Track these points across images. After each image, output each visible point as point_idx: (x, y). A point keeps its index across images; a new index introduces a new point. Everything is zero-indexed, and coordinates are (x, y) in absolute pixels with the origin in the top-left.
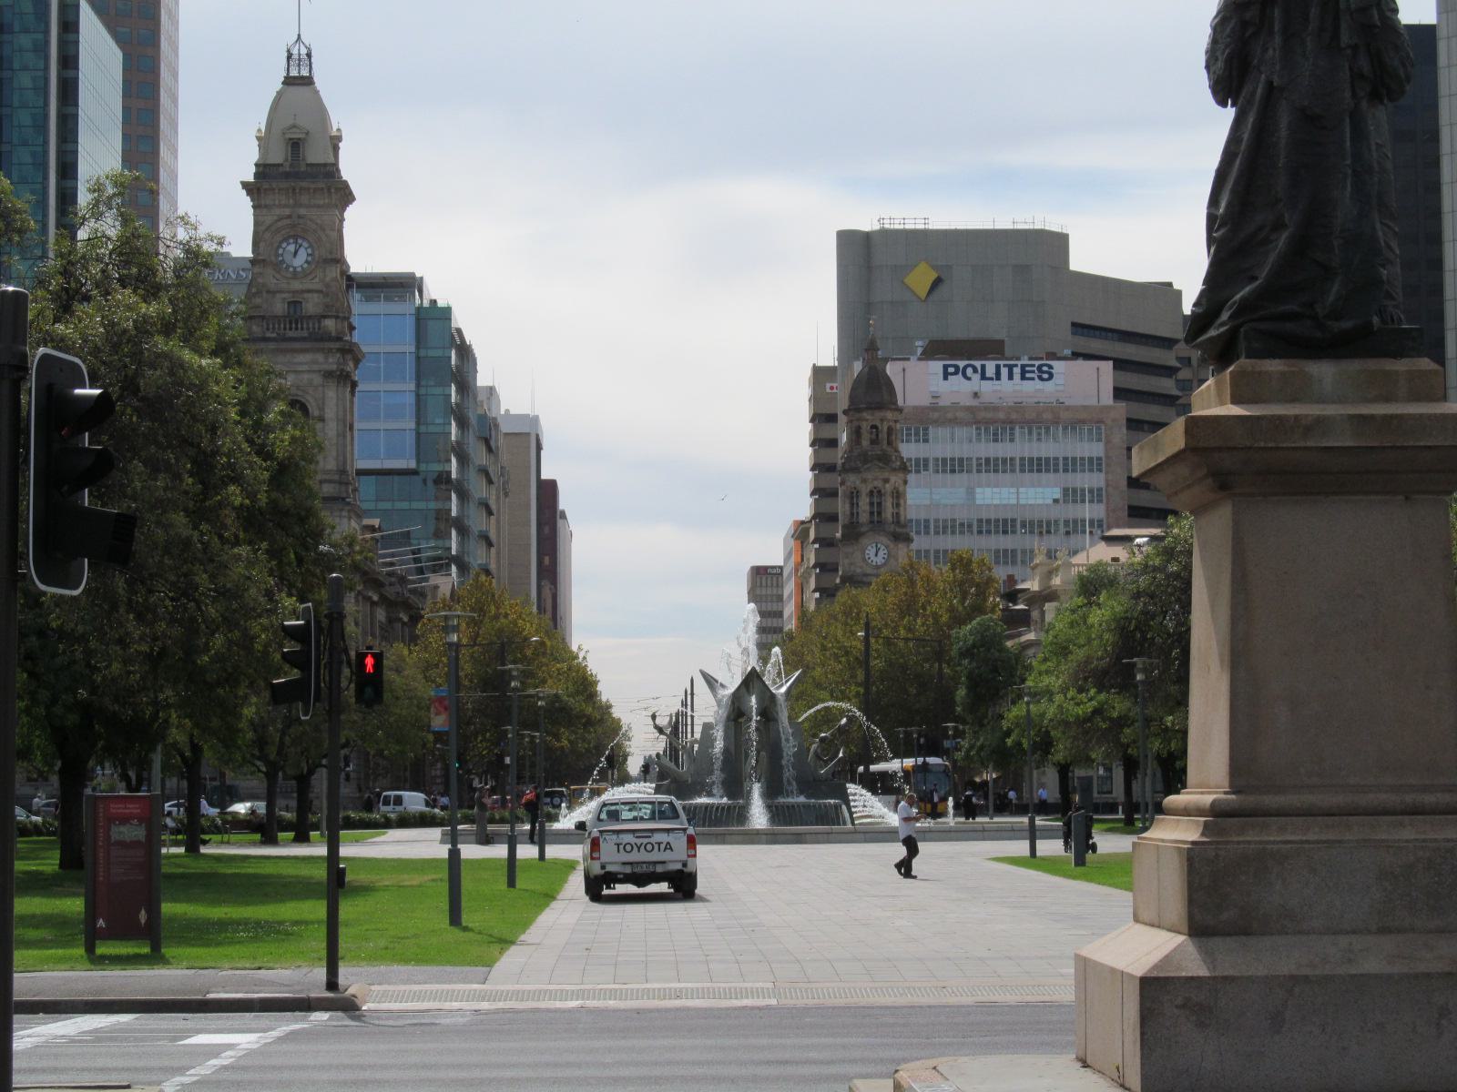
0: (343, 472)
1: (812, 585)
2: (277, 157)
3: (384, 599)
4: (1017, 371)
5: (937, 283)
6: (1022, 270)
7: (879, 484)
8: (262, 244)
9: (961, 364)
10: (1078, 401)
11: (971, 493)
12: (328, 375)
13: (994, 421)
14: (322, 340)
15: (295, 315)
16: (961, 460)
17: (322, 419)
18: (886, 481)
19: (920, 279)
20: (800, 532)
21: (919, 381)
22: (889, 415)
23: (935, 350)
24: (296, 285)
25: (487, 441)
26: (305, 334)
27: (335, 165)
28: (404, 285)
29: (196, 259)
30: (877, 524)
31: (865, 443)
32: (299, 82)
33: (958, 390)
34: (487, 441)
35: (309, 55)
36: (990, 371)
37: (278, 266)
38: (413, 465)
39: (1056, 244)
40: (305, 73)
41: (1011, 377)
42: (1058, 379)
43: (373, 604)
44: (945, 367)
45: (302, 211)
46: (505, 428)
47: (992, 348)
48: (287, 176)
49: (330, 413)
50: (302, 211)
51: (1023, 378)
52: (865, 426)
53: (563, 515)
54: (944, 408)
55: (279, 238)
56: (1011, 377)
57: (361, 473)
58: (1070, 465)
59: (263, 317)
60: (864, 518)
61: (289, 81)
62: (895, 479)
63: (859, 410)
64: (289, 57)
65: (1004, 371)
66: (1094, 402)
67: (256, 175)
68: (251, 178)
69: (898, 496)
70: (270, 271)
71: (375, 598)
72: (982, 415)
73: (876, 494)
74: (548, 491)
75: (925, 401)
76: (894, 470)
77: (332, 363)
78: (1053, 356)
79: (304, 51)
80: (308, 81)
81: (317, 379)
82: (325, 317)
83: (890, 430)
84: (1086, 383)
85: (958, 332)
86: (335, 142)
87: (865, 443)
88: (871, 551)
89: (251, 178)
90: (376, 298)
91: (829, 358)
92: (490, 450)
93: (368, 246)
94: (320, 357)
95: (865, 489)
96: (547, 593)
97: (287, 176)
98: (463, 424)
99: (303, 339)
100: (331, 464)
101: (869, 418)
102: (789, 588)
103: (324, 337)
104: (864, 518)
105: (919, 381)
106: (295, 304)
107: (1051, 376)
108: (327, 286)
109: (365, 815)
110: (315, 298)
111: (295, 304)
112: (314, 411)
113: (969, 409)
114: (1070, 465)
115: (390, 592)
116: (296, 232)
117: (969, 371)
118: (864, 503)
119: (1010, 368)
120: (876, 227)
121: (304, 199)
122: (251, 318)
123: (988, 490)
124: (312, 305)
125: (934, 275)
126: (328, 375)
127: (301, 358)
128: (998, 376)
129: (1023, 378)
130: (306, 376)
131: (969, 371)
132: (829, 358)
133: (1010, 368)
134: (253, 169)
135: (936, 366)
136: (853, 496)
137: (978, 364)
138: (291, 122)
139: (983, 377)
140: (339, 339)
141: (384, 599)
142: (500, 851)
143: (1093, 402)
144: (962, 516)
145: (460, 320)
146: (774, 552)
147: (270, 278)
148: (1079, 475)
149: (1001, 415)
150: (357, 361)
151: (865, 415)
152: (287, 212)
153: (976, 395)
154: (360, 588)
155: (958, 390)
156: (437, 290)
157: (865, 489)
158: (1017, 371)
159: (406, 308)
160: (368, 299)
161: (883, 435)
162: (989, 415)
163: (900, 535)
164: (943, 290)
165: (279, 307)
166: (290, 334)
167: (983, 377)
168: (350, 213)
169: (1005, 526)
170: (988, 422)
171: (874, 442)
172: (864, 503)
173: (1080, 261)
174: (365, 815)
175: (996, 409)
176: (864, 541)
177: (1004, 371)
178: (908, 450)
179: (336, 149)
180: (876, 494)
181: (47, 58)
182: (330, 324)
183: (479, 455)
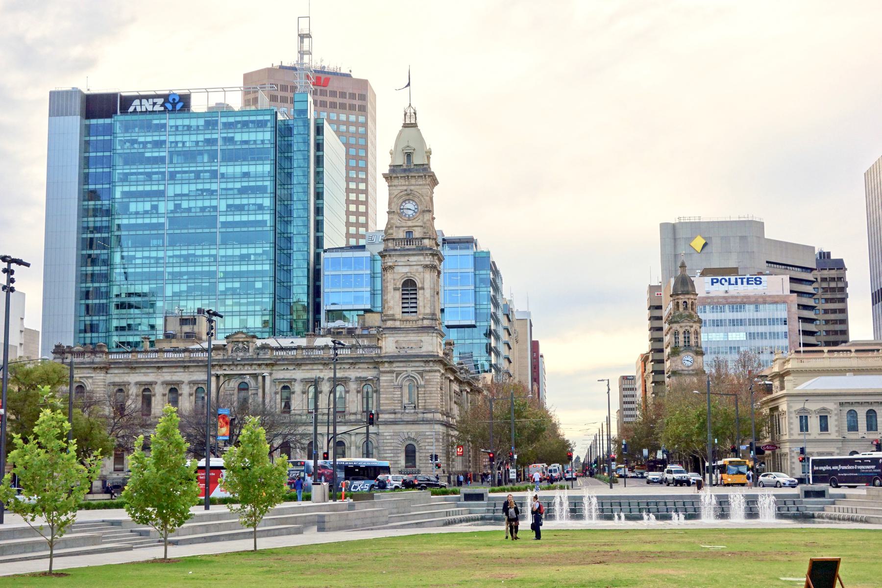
1: (651, 380)
2: (401, 160)
3: (456, 379)
4: (745, 280)
5: (705, 245)
7: (688, 328)
8: (393, 205)
9: (720, 278)
13: (736, 303)
14: (422, 250)
15: (409, 239)
16: (721, 320)
17: (423, 288)
18: (692, 327)
20: (645, 359)
22: (692, 297)
24: (410, 223)
25: (508, 316)
26: (414, 247)
27: (428, 165)
28: (468, 242)
30: (688, 347)
31: (681, 309)
32: (410, 125)
33: (718, 290)
34: (508, 316)
35: (415, 113)
36: (733, 281)
38: (473, 323)
40: (413, 122)
41: (742, 283)
43: (451, 381)
44: (712, 280)
45: (412, 188)
48: (405, 170)
50: (412, 188)
51: (748, 283)
52: (681, 302)
53: (542, 356)
54: (712, 297)
55: (401, 201)
56: (742, 283)
57: (448, 327)
59: (393, 239)
60: (681, 344)
61: (405, 126)
63: (678, 295)
64: (405, 114)
65: (739, 281)
66: (781, 293)
67: (390, 170)
68: (387, 172)
69: (697, 333)
71: (452, 378)
72: (730, 300)
76: (695, 322)
77: (428, 260)
78: (761, 273)
79: (412, 111)
80: (414, 125)
81: (420, 269)
82: (423, 238)
83: (692, 304)
84: (777, 284)
85: (715, 265)
86: (429, 153)
87: (681, 309)
89: (387, 172)
92: (509, 320)
94: (421, 258)
95: (681, 331)
96: (535, 387)
98: (496, 305)
99: (414, 249)
101: (682, 298)
102: (639, 383)
103: (423, 248)
104: (681, 344)
107: (761, 283)
108: (425, 223)
109: (769, 397)
112: (419, 285)
113: (724, 297)
115: (461, 377)
116: (409, 196)
117: (723, 281)
118: (681, 337)
119: (742, 279)
120: (677, 221)
121: (413, 181)
122: (388, 240)
123: (734, 334)
125: (704, 242)
126: (426, 266)
127: (412, 259)
128: (736, 283)
129: (748, 283)
130: (415, 267)
131: (723, 281)
133: (742, 279)
134: (388, 168)
135: (708, 279)
136: (676, 334)
137: (727, 278)
138: (406, 144)
139: (730, 284)
140: (431, 249)
141: (456, 379)
145: (494, 258)
146: (633, 371)
148: (776, 326)
149: (739, 300)
151: (680, 297)
152: (405, 188)
153: (726, 292)
154: (443, 371)
155: (718, 290)
157: (681, 331)
158: (745, 280)
159: (470, 252)
160: (452, 249)
161: (689, 306)
162: (734, 300)
165: (402, 235)
166: (407, 247)
167: (730, 284)
170: (733, 303)
171: (686, 308)
172: (681, 337)
174: (769, 397)
175: (737, 297)
176: (682, 355)
177: (739, 281)
179: (428, 158)
181: (309, 145)
182: (426, 242)
183: (504, 321)
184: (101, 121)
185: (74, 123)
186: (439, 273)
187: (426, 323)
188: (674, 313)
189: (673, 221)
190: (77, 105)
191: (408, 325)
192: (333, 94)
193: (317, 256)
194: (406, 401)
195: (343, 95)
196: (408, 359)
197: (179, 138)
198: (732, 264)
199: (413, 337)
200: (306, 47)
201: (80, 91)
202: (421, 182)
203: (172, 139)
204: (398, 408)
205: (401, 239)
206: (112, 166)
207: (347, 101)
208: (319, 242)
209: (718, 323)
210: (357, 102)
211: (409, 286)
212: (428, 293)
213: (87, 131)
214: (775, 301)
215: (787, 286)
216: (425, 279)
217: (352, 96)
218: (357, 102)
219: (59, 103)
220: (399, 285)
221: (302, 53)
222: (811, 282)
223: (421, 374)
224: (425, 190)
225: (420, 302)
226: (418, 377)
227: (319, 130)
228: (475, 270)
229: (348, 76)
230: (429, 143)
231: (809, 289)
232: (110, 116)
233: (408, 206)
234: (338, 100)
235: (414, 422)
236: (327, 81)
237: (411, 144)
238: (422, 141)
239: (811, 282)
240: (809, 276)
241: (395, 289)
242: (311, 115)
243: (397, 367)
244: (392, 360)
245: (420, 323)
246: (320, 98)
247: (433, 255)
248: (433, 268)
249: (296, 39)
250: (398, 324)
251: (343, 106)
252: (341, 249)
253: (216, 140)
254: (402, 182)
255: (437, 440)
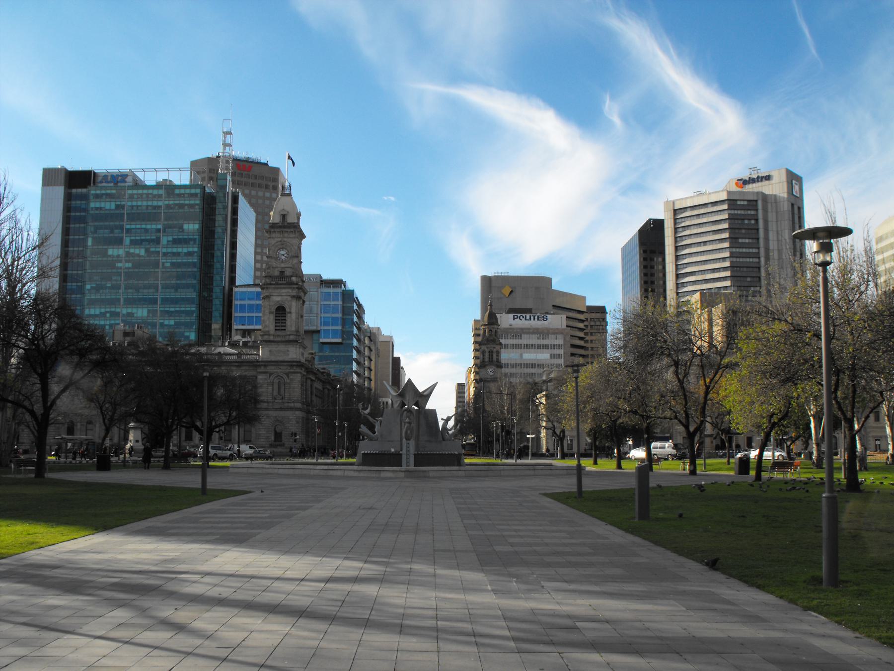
0: (297, 331)
5: (511, 292)
6: (537, 289)
10: (556, 327)
11: (521, 355)
12: (293, 297)
19: (506, 291)
21: (506, 320)
23: (510, 311)
24: (283, 265)
27: (298, 223)
28: (338, 283)
29: (433, 413)
30: (491, 361)
36: (528, 318)
37: (277, 258)
38: (340, 340)
39: (548, 281)
42: (549, 320)
46: (381, 339)
47: (529, 311)
48: (280, 227)
49: (293, 310)
58: (553, 346)
62: (498, 347)
69: (498, 353)
70: (273, 260)
73: (491, 352)
74: (397, 361)
75: (508, 326)
77: (294, 293)
81: (289, 298)
84: (557, 321)
86: (299, 215)
88: (489, 371)
90: (329, 287)
91: (478, 317)
93: (315, 261)
94: (290, 291)
95: (487, 350)
97: (280, 227)
100: (293, 329)
104: (487, 360)
105: (506, 320)
106: (282, 272)
110: (289, 270)
111: (282, 272)
112: (288, 310)
114: (553, 346)
121: (286, 235)
124: (288, 272)
126: (293, 297)
127: (284, 291)
132: (478, 317)
135: (511, 316)
142: (572, 463)
143: (559, 327)
144: (518, 362)
147: (273, 263)
150: (305, 293)
155: (520, 323)
156: (350, 286)
163: (499, 365)
164: (513, 294)
165: (277, 273)
168: (304, 241)
169: (533, 366)
172: (487, 355)
173: (555, 286)
178: (503, 341)
179: (299, 219)
180: (491, 352)
182: (294, 279)
184: (79, 190)
185: (59, 191)
186: (304, 302)
187: (292, 338)
188: (488, 342)
189: (490, 275)
190: (62, 178)
191: (279, 339)
192: (254, 177)
193: (231, 290)
194: (275, 393)
195: (261, 178)
196: (277, 363)
197: (134, 203)
198: (529, 305)
199: (282, 348)
200: (228, 141)
201: (66, 170)
202: (292, 235)
203: (130, 204)
204: (270, 399)
205: (277, 277)
206: (85, 222)
207: (264, 182)
208: (232, 280)
209: (514, 346)
210: (271, 184)
211: (281, 312)
212: (294, 316)
213: (68, 197)
214: (556, 332)
215: (564, 322)
216: (293, 307)
217: (268, 179)
218: (271, 184)
219: (50, 176)
220: (273, 309)
221: (225, 145)
222: (582, 321)
223: (287, 374)
224: (295, 241)
225: (288, 323)
226: (285, 376)
227: (235, 200)
228: (343, 303)
229: (266, 164)
230: (300, 208)
231: (581, 325)
232: (85, 187)
233: (282, 252)
234: (257, 181)
235: (281, 409)
236: (250, 169)
237: (286, 208)
238: (294, 206)
239: (582, 321)
240: (582, 317)
241: (270, 313)
242: (230, 188)
243: (270, 369)
244: (266, 363)
245: (287, 338)
246: (237, 178)
247: (298, 288)
248: (298, 298)
249: (222, 135)
250: (272, 338)
251: (261, 186)
252: (249, 286)
253: (161, 207)
254: (278, 235)
255: (298, 422)
